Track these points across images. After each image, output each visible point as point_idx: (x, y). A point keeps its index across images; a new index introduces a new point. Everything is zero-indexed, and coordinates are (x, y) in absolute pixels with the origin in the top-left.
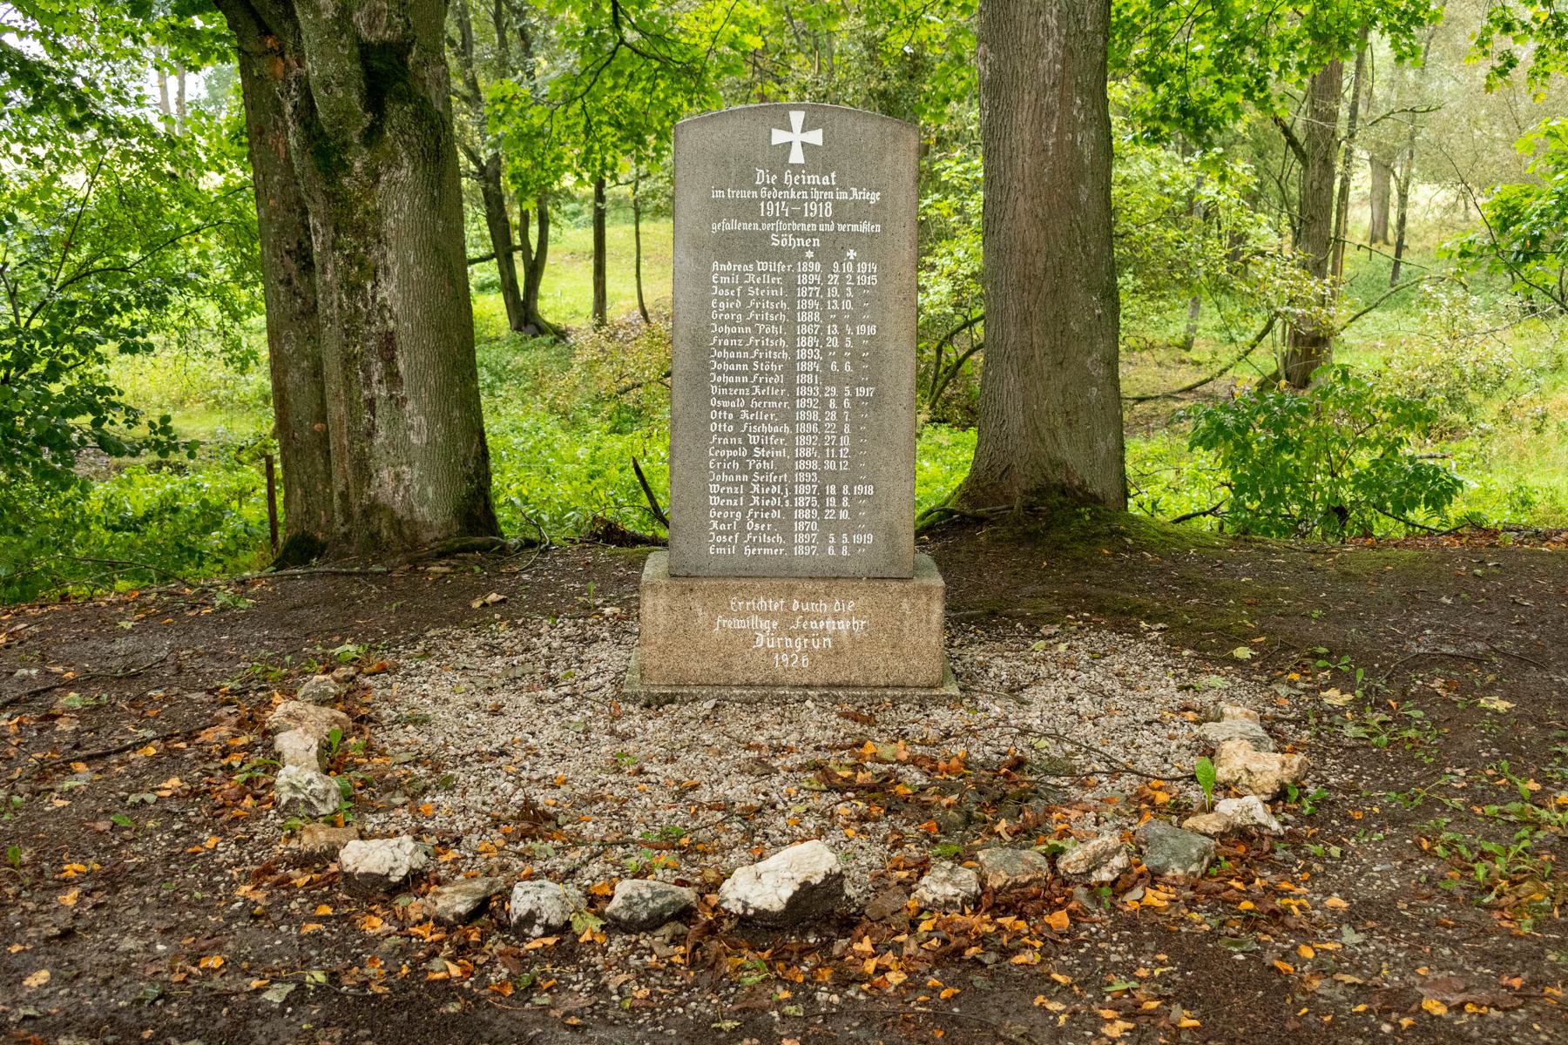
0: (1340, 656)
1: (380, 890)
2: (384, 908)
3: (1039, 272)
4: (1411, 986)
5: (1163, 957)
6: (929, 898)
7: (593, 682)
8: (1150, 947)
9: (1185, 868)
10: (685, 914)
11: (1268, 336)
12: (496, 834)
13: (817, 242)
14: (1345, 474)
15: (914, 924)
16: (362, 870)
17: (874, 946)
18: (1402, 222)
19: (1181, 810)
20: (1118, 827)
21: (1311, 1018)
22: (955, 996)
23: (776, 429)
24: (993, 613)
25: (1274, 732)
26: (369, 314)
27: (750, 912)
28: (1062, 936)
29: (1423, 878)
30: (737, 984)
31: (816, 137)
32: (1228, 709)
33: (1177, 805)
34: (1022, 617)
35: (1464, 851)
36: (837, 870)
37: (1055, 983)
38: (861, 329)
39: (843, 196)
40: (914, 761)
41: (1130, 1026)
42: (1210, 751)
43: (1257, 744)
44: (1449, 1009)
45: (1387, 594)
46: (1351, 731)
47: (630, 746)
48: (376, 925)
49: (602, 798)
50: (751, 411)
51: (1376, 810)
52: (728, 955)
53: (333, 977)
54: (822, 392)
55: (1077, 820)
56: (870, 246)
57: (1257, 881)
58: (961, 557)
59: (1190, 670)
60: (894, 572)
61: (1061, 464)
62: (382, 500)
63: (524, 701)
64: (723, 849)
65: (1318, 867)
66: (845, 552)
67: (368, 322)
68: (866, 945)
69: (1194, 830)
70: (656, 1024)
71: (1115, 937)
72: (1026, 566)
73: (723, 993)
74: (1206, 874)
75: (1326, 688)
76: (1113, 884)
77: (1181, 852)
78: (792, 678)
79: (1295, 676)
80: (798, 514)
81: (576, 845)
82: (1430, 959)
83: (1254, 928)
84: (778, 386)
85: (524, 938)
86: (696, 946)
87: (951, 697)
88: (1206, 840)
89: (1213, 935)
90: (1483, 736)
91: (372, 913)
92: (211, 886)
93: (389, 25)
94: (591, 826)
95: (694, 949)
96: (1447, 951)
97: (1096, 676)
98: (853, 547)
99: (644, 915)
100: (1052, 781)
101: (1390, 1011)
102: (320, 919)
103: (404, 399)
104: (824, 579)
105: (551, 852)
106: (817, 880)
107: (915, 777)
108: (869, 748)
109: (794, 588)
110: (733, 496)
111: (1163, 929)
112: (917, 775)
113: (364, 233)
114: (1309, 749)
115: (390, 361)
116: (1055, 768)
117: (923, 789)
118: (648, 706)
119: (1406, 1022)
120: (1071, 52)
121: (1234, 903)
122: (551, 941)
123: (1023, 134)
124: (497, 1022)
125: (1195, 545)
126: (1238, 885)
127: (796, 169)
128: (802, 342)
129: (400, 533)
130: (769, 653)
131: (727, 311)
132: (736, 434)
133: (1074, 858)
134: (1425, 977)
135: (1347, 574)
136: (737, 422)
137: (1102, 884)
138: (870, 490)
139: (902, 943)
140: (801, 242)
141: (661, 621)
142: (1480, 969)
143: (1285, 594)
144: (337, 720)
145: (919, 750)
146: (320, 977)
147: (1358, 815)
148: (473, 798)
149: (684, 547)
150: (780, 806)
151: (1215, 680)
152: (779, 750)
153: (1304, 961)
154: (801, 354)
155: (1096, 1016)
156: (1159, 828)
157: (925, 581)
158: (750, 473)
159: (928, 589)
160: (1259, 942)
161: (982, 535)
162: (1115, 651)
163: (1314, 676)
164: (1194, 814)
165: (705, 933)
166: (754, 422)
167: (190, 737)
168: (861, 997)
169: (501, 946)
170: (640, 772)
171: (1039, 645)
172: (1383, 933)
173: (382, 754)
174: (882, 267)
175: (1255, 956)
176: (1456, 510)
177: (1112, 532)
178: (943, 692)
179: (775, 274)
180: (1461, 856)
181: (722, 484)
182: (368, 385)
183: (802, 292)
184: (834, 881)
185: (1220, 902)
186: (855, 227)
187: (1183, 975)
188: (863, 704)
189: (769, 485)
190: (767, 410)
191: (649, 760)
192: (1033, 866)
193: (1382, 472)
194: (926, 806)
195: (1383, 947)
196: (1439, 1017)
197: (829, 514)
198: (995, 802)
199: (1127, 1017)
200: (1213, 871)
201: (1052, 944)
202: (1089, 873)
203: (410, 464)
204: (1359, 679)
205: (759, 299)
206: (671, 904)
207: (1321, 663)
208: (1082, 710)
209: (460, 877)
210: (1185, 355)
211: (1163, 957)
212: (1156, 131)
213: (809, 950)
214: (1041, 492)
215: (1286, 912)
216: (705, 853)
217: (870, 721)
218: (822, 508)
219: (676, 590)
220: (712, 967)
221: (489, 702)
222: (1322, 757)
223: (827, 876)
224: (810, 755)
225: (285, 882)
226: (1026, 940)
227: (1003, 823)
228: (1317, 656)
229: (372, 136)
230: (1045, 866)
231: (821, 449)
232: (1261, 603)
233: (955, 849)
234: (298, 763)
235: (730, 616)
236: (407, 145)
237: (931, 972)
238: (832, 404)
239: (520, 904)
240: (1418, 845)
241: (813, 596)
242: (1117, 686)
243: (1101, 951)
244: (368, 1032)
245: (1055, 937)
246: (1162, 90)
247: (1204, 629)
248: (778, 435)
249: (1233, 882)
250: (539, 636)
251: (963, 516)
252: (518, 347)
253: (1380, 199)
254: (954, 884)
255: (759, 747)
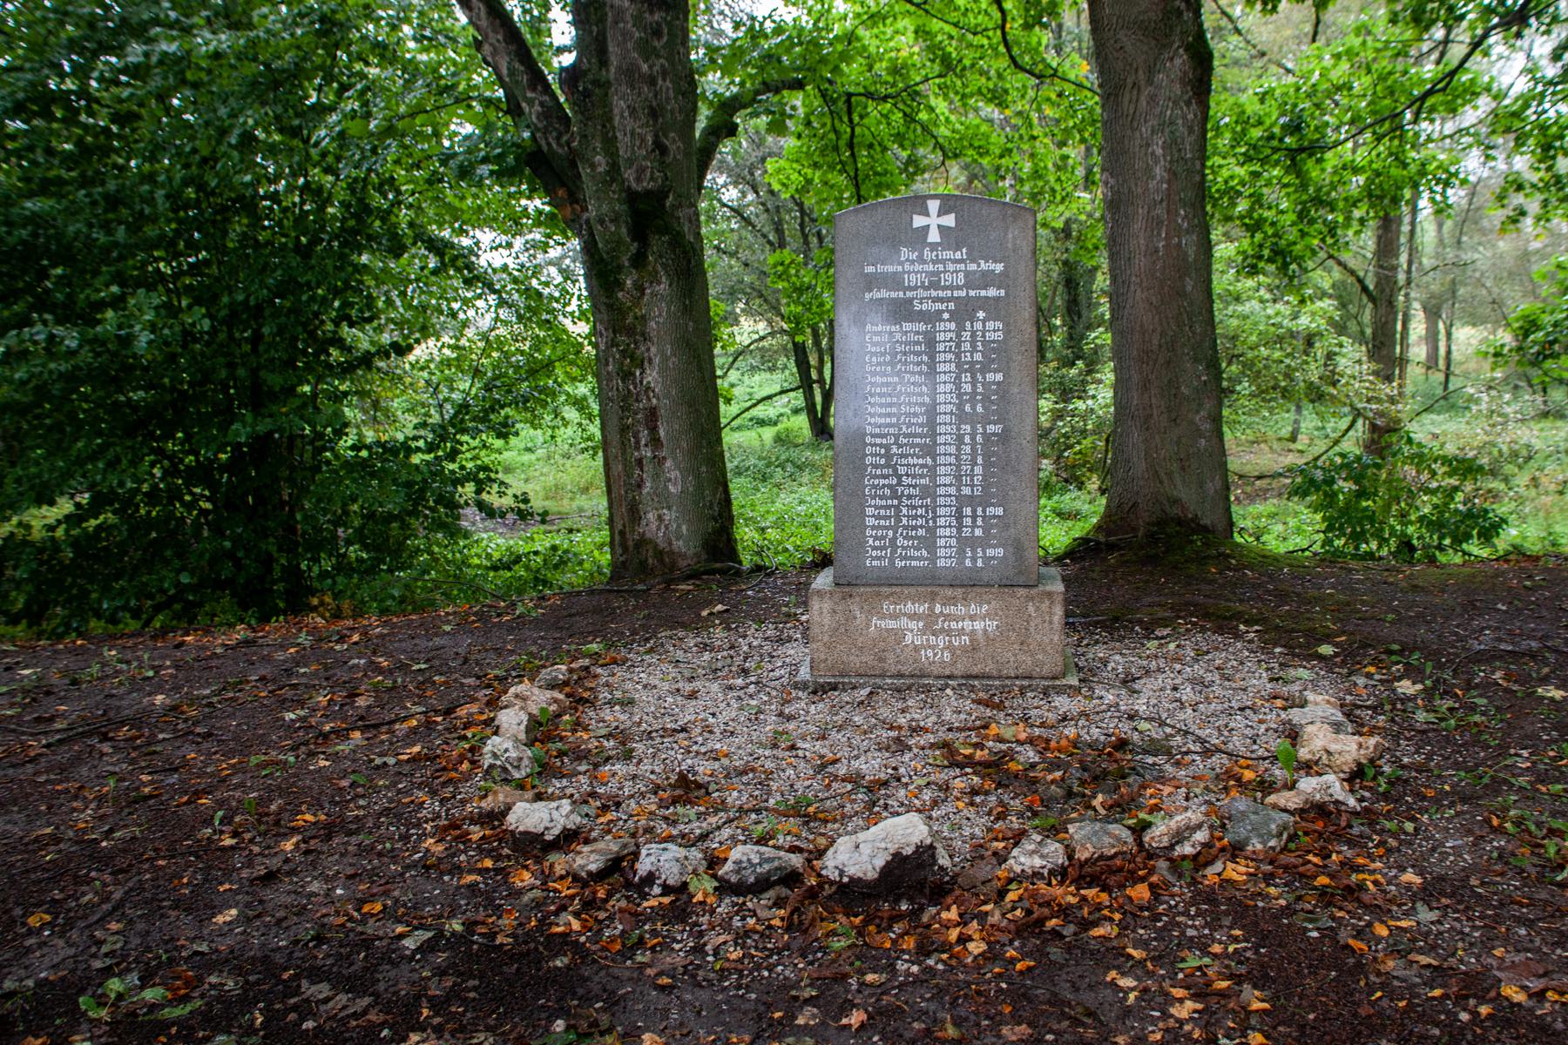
0: (1411, 652)
1: (534, 846)
2: (536, 862)
3: (1155, 348)
4: (1488, 968)
5: (1237, 932)
6: (1018, 869)
7: (777, 673)
8: (1227, 921)
9: (1264, 843)
10: (791, 878)
11: (1351, 433)
12: (654, 799)
13: (952, 306)
14: (1413, 518)
15: (1002, 893)
16: (521, 829)
17: (961, 915)
18: (1449, 352)
19: (1267, 786)
20: (1206, 802)
21: (1385, 1003)
22: (1029, 969)
23: (921, 461)
24: (1116, 619)
25: (1353, 717)
26: (638, 394)
27: (846, 880)
28: (1141, 909)
29: (1495, 854)
30: (824, 949)
31: (949, 220)
32: (1310, 696)
33: (1262, 782)
34: (1140, 622)
35: (1533, 828)
36: (928, 841)
37: (1130, 957)
38: (990, 377)
39: (973, 267)
40: (1031, 741)
41: (1199, 1006)
42: (1293, 735)
43: (1337, 728)
44: (1530, 996)
45: (1451, 602)
46: (1421, 716)
47: (791, 726)
48: (525, 879)
49: (753, 770)
50: (900, 446)
51: (1447, 788)
52: (822, 920)
53: (470, 926)
54: (959, 429)
55: (1169, 795)
56: (994, 308)
57: (1334, 856)
58: (1095, 575)
59: (1281, 664)
60: (1021, 581)
61: (1176, 501)
62: (648, 535)
63: (715, 687)
64: (843, 816)
65: (1392, 842)
66: (980, 563)
67: (637, 401)
68: (952, 914)
69: (1275, 806)
70: (739, 987)
71: (1193, 911)
72: (1147, 582)
73: (810, 957)
74: (1285, 849)
75: (1399, 679)
76: (1195, 857)
77: (1262, 824)
78: (936, 670)
79: (1372, 669)
80: (940, 532)
81: (716, 811)
82: (1506, 941)
83: (1329, 904)
84: (921, 425)
85: (645, 896)
86: (796, 910)
87: (1071, 687)
88: (1285, 816)
89: (1288, 911)
90: (1543, 721)
91: (526, 867)
92: (405, 838)
93: (652, 179)
94: (735, 794)
95: (792, 914)
96: (1523, 932)
97: (1198, 670)
98: (986, 559)
99: (752, 879)
100: (1150, 760)
101: (1467, 997)
102: (481, 872)
103: (664, 458)
104: (962, 586)
105: (693, 817)
106: (908, 851)
107: (1030, 755)
108: (994, 729)
109: (936, 594)
110: (886, 518)
111: (1240, 903)
112: (1031, 754)
113: (635, 334)
114: (1383, 732)
115: (653, 430)
116: (1155, 748)
117: (1033, 766)
118: (815, 692)
119: (1484, 1010)
120: (1175, 174)
121: (1308, 877)
122: (666, 900)
123: (1138, 239)
124: (596, 979)
125: (1290, 565)
126: (1315, 860)
127: (934, 247)
128: (941, 389)
129: (661, 561)
130: (916, 649)
131: (879, 364)
132: (887, 466)
133: (1160, 832)
134: (1502, 959)
135: (1416, 586)
136: (888, 456)
137: (1184, 857)
138: (1000, 511)
139: (987, 913)
140: (939, 306)
141: (826, 621)
142: (1559, 951)
143: (1363, 603)
144: (556, 701)
145: (1037, 731)
146: (458, 928)
147: (1430, 793)
148: (646, 767)
149: (845, 560)
150: (904, 780)
151: (1303, 673)
152: (916, 730)
153: (1379, 940)
154: (941, 398)
155: (1167, 994)
156: (1242, 804)
157: (1048, 588)
158: (899, 498)
159: (1050, 594)
160: (1333, 918)
161: (1112, 559)
162: (1217, 649)
163: (1388, 669)
164: (1278, 790)
165: (805, 898)
166: (902, 456)
167: (448, 712)
168: (940, 967)
169: (623, 903)
170: (793, 747)
171: (1152, 645)
172: (1457, 911)
173: (586, 729)
174: (1006, 325)
175: (1330, 934)
176: (1502, 543)
177: (1220, 555)
178: (1064, 682)
179: (918, 333)
180: (1530, 833)
181: (876, 507)
182: (638, 448)
183: (941, 347)
184: (925, 854)
185: (1298, 876)
186: (983, 293)
187: (1257, 952)
188: (993, 690)
189: (915, 507)
190: (913, 446)
191: (803, 738)
192: (1118, 839)
193: (1441, 513)
194: (1035, 781)
195: (1458, 925)
196: (1519, 1005)
197: (966, 532)
198: (1095, 778)
199: (1195, 997)
200: (1292, 846)
201: (1131, 916)
202: (1172, 847)
203: (669, 508)
204: (1428, 671)
205: (905, 353)
206: (777, 869)
207: (1394, 658)
208: (1184, 698)
209: (609, 837)
210: (1292, 446)
211: (1237, 932)
212: (1254, 266)
213: (898, 917)
214: (1162, 523)
215: (1361, 887)
216: (826, 821)
217: (1000, 707)
218: (960, 528)
219: (837, 596)
220: (805, 932)
221: (688, 687)
222: (1396, 738)
223: (918, 847)
224: (943, 735)
225: (464, 838)
226: (1105, 912)
227: (1100, 798)
228: (1390, 652)
229: (639, 261)
230: (1130, 840)
231: (958, 478)
232: (1342, 611)
233: (1052, 821)
234: (508, 737)
235: (883, 618)
236: (664, 266)
237: (1011, 942)
238: (967, 439)
239: (644, 866)
240: (1487, 821)
241: (953, 601)
242: (1217, 678)
243: (1178, 924)
244: (477, 982)
245: (1135, 910)
246: (1259, 237)
247: (1293, 630)
248: (922, 466)
249: (1310, 857)
250: (745, 637)
251: (1098, 543)
252: (815, 447)
253: (1432, 338)
254: (1042, 857)
255: (900, 728)
